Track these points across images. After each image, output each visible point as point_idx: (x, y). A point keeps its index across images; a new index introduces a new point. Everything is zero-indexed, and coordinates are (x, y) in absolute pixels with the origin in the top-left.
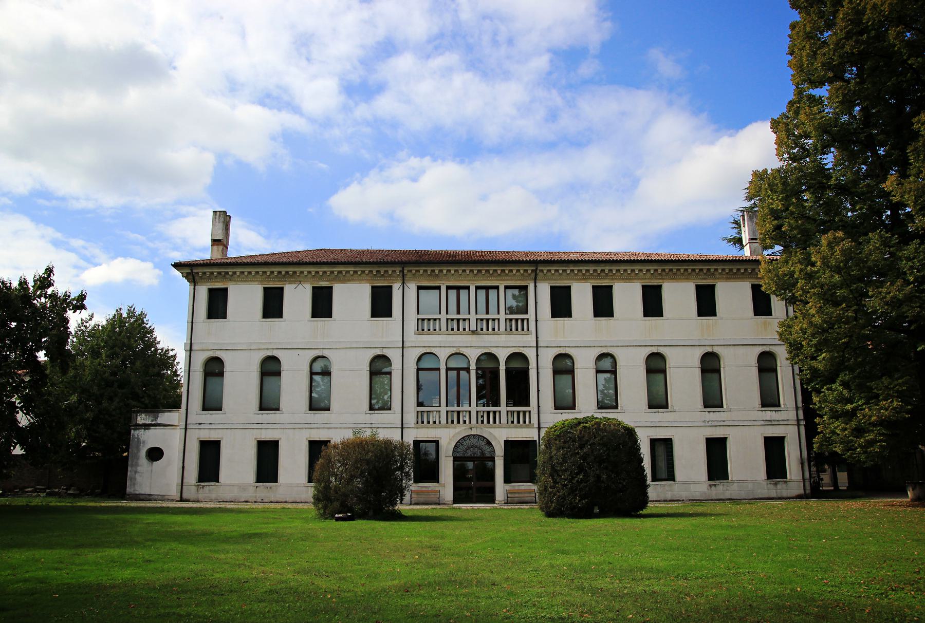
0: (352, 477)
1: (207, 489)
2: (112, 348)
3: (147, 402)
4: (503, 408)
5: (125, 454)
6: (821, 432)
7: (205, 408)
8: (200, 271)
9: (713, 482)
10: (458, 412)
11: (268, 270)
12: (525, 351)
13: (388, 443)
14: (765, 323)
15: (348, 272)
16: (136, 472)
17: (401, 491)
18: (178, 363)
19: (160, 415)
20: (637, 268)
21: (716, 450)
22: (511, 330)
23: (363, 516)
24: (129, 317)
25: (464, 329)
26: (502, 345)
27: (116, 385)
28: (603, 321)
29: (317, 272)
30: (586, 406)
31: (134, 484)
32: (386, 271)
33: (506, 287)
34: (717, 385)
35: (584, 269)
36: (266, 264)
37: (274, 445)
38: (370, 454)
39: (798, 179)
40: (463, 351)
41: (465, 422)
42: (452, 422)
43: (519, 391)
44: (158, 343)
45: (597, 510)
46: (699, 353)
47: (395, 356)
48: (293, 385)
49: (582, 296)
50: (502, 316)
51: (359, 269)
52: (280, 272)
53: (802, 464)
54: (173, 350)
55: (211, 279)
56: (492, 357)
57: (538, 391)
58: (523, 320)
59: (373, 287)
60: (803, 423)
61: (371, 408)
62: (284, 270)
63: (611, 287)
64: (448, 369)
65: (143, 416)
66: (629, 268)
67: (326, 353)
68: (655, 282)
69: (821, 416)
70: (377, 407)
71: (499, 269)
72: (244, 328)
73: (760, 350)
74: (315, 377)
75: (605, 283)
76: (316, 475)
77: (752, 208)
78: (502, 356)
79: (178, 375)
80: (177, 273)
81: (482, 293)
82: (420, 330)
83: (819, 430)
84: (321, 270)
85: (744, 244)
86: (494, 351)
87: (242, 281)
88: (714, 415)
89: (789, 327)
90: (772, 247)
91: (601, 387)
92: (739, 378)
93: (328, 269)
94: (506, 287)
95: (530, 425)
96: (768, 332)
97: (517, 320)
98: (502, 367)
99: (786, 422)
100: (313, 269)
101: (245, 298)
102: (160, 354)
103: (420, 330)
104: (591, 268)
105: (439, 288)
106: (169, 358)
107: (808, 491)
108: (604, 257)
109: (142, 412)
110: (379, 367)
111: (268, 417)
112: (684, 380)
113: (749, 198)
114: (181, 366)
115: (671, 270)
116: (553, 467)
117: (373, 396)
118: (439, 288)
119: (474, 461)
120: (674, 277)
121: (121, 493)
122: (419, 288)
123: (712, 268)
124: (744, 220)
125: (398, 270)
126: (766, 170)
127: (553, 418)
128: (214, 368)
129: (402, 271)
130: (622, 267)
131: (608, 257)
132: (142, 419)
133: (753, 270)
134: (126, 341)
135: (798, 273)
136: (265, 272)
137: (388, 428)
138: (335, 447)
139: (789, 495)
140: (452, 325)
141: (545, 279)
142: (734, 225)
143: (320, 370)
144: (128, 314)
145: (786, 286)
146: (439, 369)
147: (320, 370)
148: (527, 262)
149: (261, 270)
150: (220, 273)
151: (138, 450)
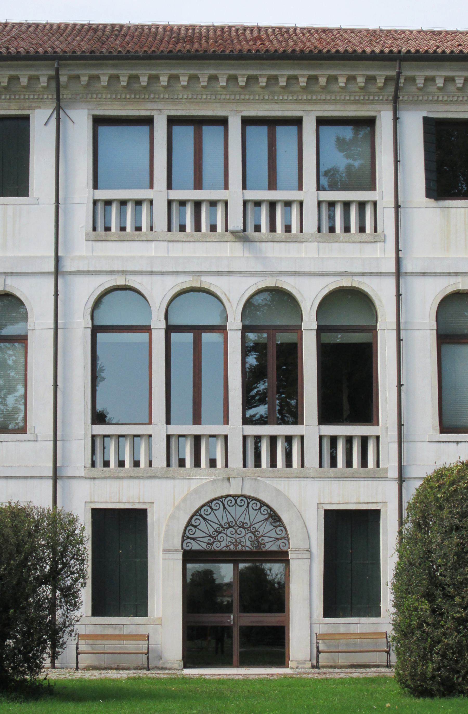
10: (197, 439)
12: (368, 285)
17: (54, 634)
22: (332, 229)
25: (213, 228)
26: (309, 267)
40: (208, 282)
41: (213, 463)
43: (350, 387)
50: (310, 194)
56: (282, 298)
57: (400, 385)
58: (362, 205)
64: (170, 329)
78: (309, 295)
81: (185, 134)
82: (100, 227)
86: (288, 284)
95: (379, 474)
97: (347, 205)
103: (100, 227)
105: (148, 121)
116: (432, 578)
118: (148, 121)
119: (236, 563)
122: (99, 121)
125: (44, 74)
140: (182, 216)
141: (415, 103)
146: (147, 329)
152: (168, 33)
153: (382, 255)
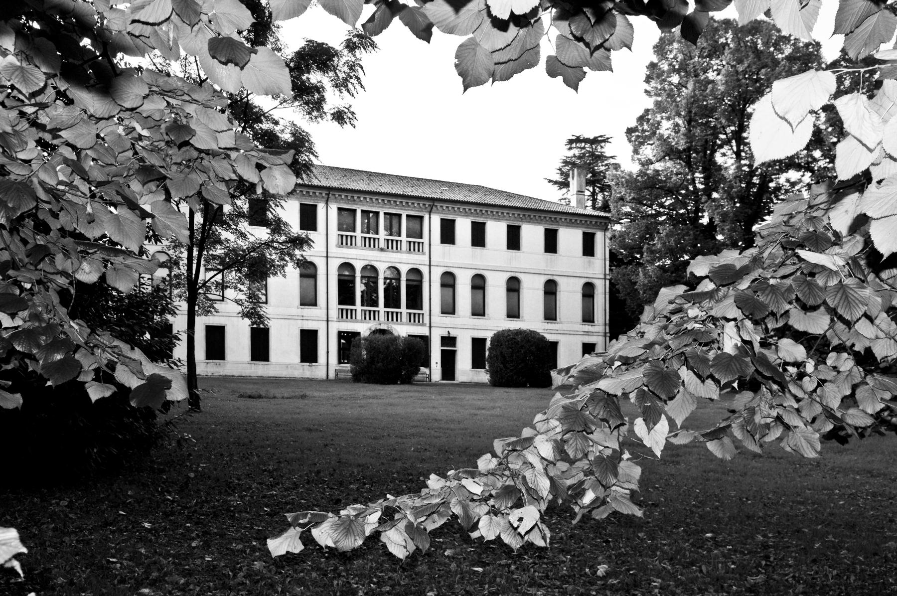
12: (421, 268)
14: (589, 262)
26: (405, 261)
46: (543, 280)
56: (374, 269)
59: (301, 204)
63: (484, 224)
68: (516, 223)
73: (509, 275)
75: (481, 220)
78: (358, 266)
86: (351, 261)
92: (570, 301)
95: (423, 324)
98: (404, 278)
120: (530, 220)
123: (558, 217)
141: (437, 212)
152: (574, 145)
153: (425, 258)
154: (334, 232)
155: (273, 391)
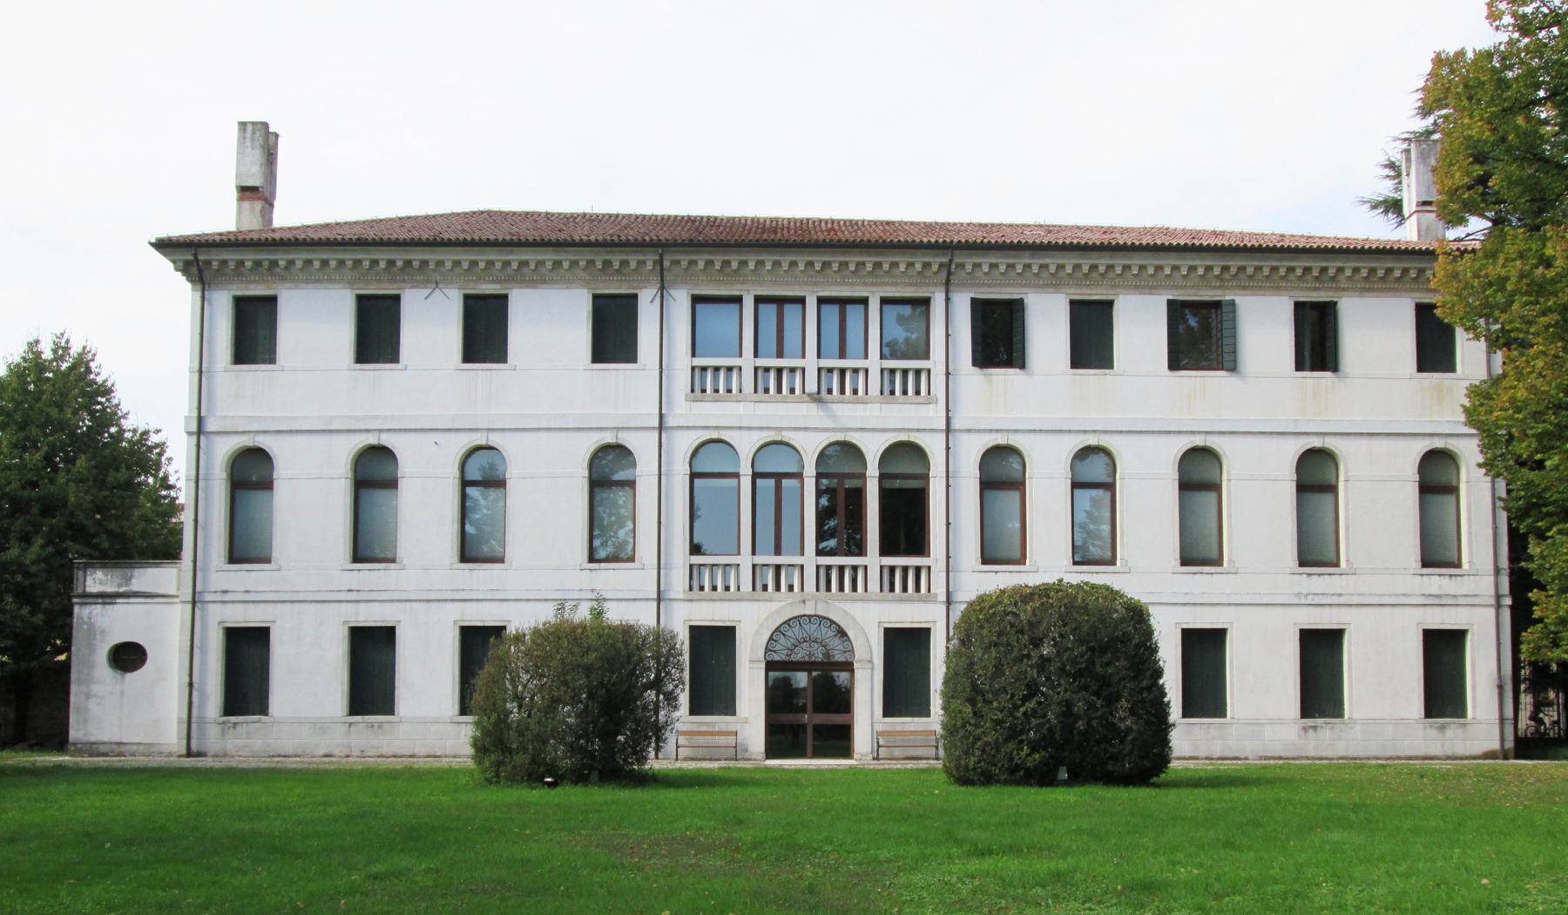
0: (555, 701)
1: (242, 730)
2: (22, 427)
3: (105, 545)
4: (873, 559)
5: (62, 657)
6: (1540, 620)
7: (233, 559)
8: (215, 257)
9: (1310, 722)
10: (778, 568)
11: (366, 256)
12: (922, 440)
13: (627, 631)
15: (540, 263)
16: (88, 696)
18: (170, 459)
19: (137, 572)
20: (1168, 262)
21: (1320, 653)
22: (892, 393)
23: (579, 777)
24: (59, 359)
26: (873, 424)
27: (36, 509)
28: (1090, 376)
29: (474, 264)
30: (1049, 562)
31: (85, 721)
32: (624, 263)
33: (884, 301)
34: (1331, 514)
35: (1052, 261)
36: (361, 243)
37: (386, 636)
38: (593, 655)
39: (1531, 72)
40: (788, 436)
41: (791, 588)
42: (765, 588)
43: (906, 525)
44: (125, 416)
45: (1063, 774)
46: (349, 447)
47: (643, 447)
48: (424, 508)
49: (1047, 326)
50: (874, 363)
51: (566, 257)
52: (391, 263)
53: (1501, 688)
54: (158, 431)
55: (243, 276)
56: (850, 450)
57: (948, 524)
58: (918, 372)
59: (596, 297)
60: (1508, 601)
61: (592, 559)
62: (400, 256)
63: (1110, 304)
64: (756, 476)
65: (99, 574)
66: (1151, 262)
67: (495, 440)
69: (1542, 588)
70: (602, 554)
71: (869, 261)
72: (316, 381)
74: (469, 490)
76: (477, 698)
77: (1428, 133)
78: (872, 447)
79: (171, 487)
80: (164, 265)
83: (1536, 615)
84: (482, 257)
85: (1406, 213)
86: (855, 438)
87: (308, 281)
88: (1319, 583)
89: (1489, 397)
90: (1461, 221)
91: (1081, 517)
93: (497, 256)
94: (884, 301)
95: (930, 598)
96: (1439, 409)
97: (905, 372)
98: (873, 471)
99: (1474, 600)
100: (465, 256)
101: (316, 322)
102: (129, 441)
103: (697, 389)
104: (1069, 261)
105: (738, 300)
106: (150, 449)
107: (1510, 744)
108: (1096, 239)
109: (93, 566)
110: (608, 471)
111: (371, 576)
112: (1258, 503)
113: (1425, 112)
114: (178, 466)
115: (1242, 269)
117: (596, 533)
118: (738, 300)
119: (809, 672)
121: (59, 741)
122: (697, 300)
123: (1332, 266)
124: (1408, 160)
126: (1461, 54)
127: (982, 583)
128: (251, 472)
129: (661, 262)
130: (1135, 261)
131: (1106, 239)
132: (97, 580)
133: (1421, 271)
134: (54, 412)
135: (1513, 280)
136: (358, 263)
137: (630, 598)
138: (519, 638)
139: (1468, 752)
140: (766, 380)
141: (964, 285)
142: (1387, 172)
143: (481, 477)
144: (55, 351)
145: (1485, 308)
146: (736, 475)
147: (481, 477)
148: (929, 246)
149: (349, 256)
150: (258, 264)
151: (92, 649)
154: (682, 362)
155: (123, 749)
